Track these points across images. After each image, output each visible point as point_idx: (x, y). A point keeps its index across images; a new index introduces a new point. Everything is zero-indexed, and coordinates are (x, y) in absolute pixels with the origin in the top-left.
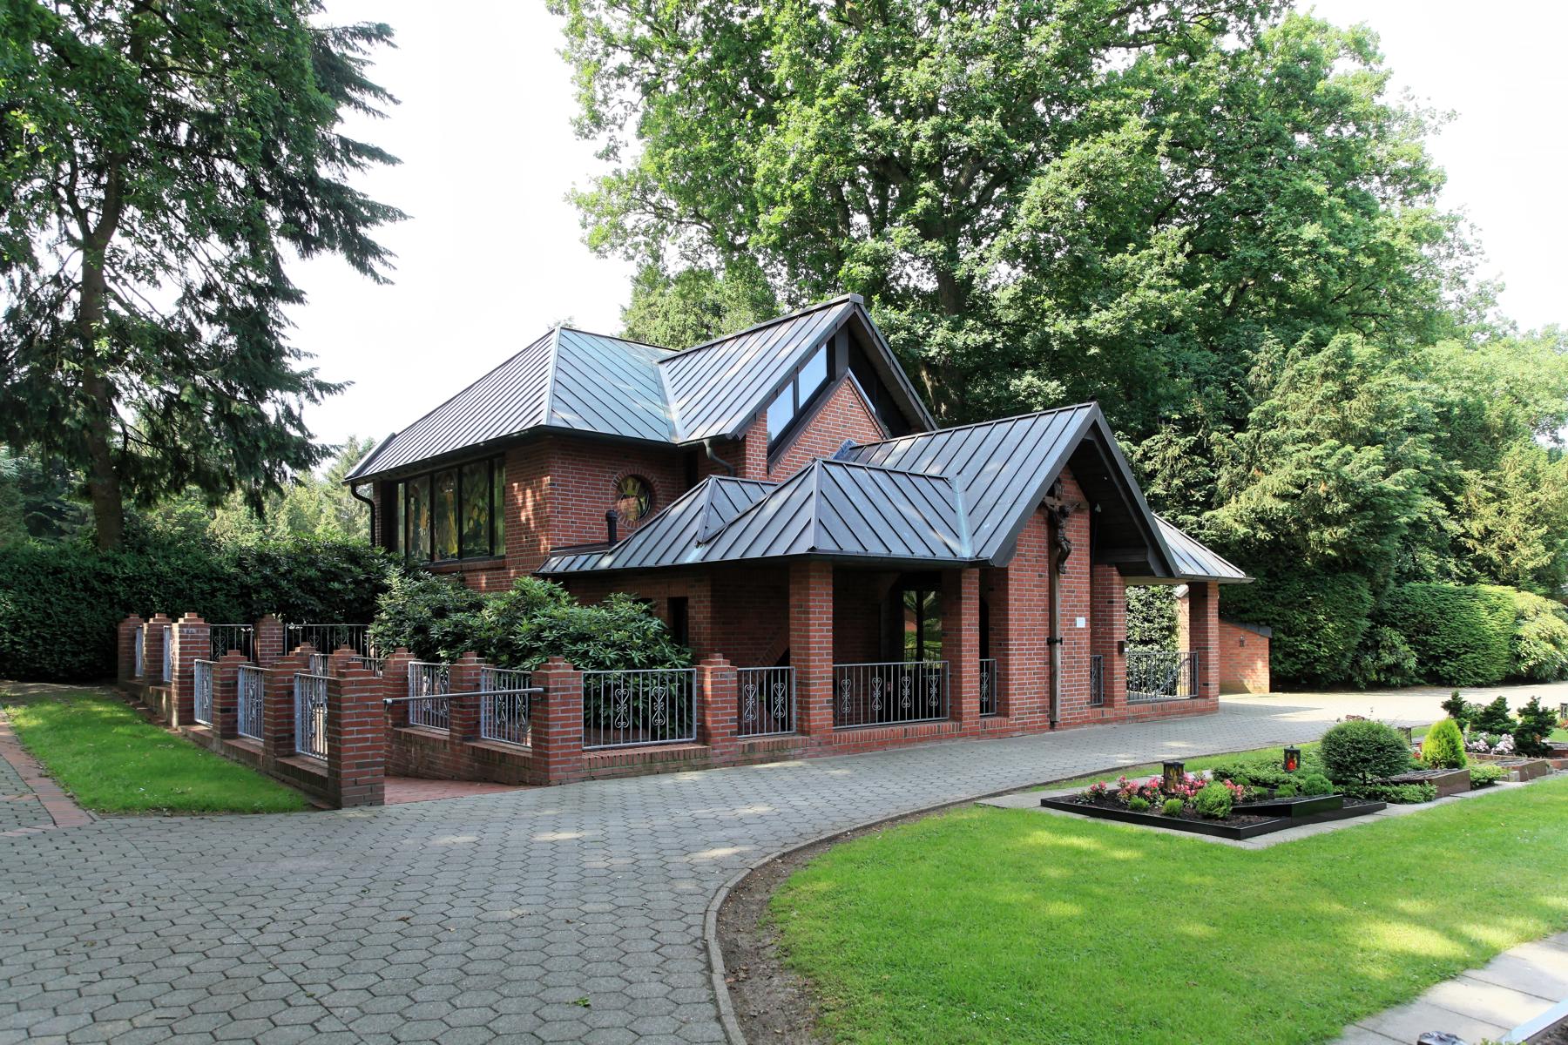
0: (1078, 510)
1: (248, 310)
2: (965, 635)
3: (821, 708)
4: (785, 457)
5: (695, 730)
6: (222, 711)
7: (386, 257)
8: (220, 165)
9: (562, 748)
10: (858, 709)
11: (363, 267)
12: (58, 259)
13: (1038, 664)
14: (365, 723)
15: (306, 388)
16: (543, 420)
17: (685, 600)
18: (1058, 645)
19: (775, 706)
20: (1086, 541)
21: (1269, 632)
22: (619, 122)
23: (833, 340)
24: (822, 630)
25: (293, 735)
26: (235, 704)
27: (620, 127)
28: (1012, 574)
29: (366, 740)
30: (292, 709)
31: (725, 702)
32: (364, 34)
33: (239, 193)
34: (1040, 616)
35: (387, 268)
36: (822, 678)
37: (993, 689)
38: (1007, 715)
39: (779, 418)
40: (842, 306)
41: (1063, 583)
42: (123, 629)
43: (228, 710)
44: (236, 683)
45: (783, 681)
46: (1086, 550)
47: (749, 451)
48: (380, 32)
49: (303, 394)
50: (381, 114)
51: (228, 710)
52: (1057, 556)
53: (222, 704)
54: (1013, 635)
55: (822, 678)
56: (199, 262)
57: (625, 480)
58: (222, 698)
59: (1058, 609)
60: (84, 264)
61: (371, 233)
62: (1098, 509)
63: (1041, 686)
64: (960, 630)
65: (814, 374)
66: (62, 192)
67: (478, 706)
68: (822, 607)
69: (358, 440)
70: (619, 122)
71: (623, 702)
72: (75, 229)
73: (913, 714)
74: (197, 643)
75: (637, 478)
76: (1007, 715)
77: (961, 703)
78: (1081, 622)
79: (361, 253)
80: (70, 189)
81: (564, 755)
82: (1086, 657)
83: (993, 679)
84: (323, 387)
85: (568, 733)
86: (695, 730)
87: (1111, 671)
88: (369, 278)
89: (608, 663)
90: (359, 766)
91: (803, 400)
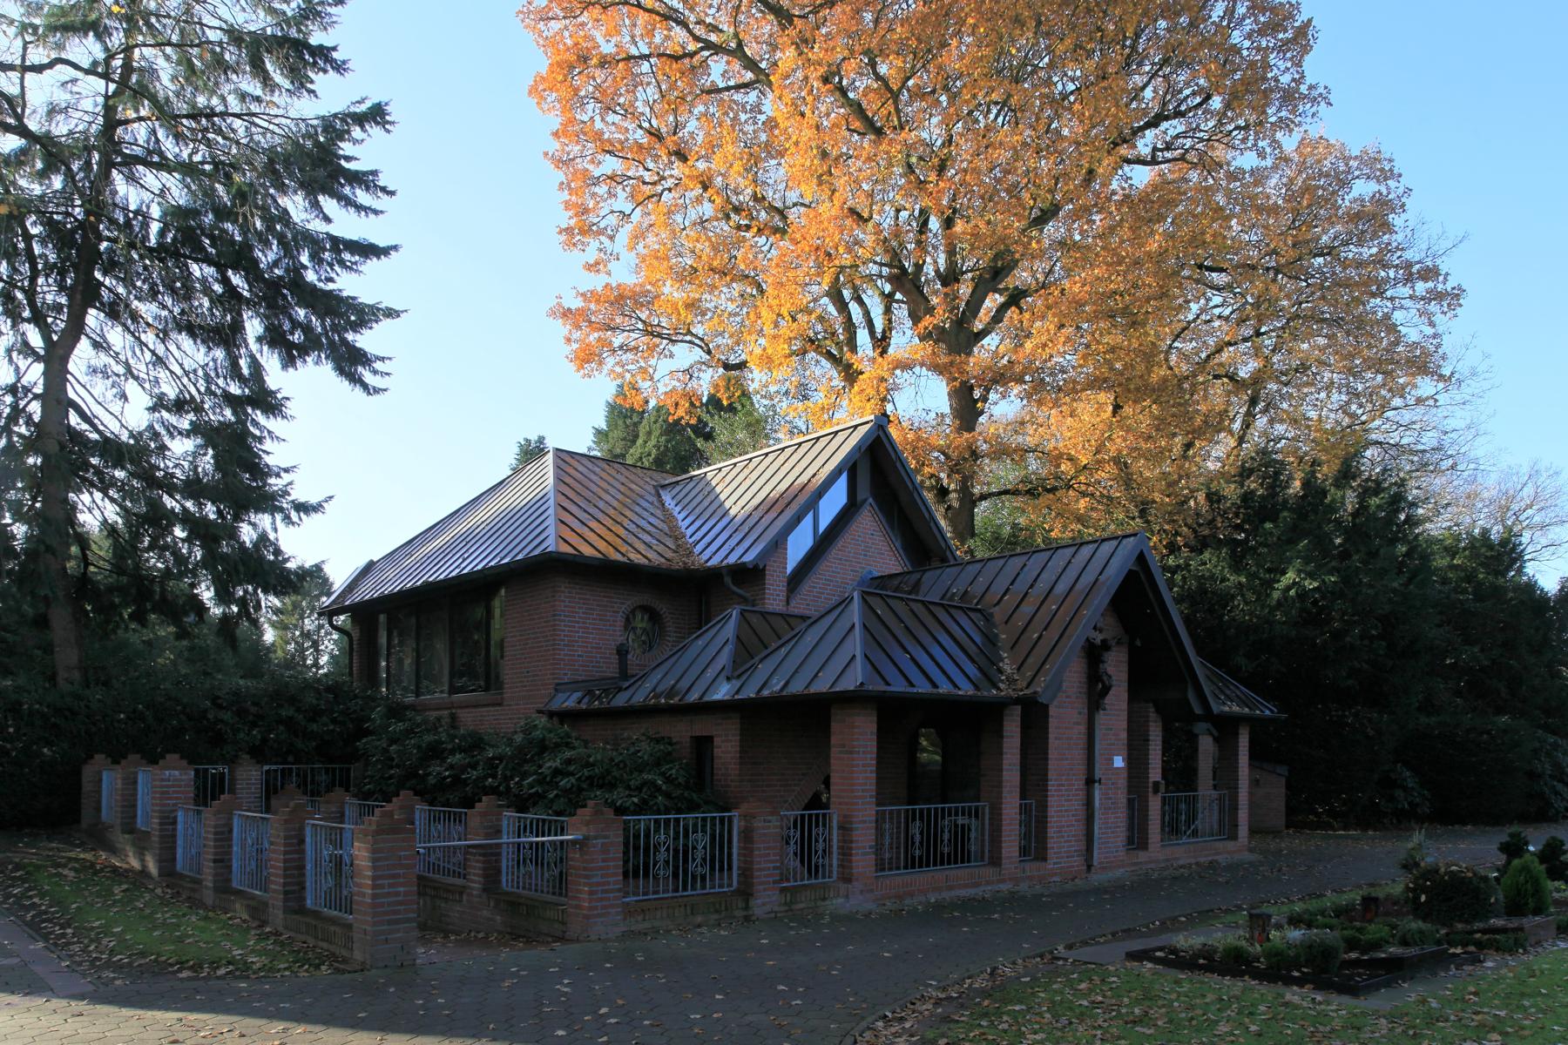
0: (1119, 643)
1: (224, 425)
2: (1006, 775)
3: (863, 854)
4: (805, 587)
5: (835, 873)
6: (215, 861)
7: (378, 365)
8: (195, 269)
9: (602, 899)
10: (898, 853)
11: (355, 380)
12: (12, 369)
13: (1077, 805)
14: (398, 876)
15: (281, 510)
16: (551, 545)
17: (710, 739)
18: (1097, 785)
19: (816, 852)
20: (1124, 676)
21: (1283, 770)
22: (609, 232)
23: (855, 464)
24: (866, 772)
25: (304, 888)
26: (230, 853)
27: (612, 238)
28: (1052, 711)
29: (398, 894)
30: (303, 859)
31: (768, 848)
32: (361, 119)
33: (216, 300)
34: (1079, 755)
35: (378, 377)
36: (865, 822)
37: (1030, 832)
38: (1045, 859)
39: (799, 544)
40: (868, 426)
41: (1101, 718)
42: (88, 772)
43: (221, 861)
44: (231, 831)
45: (824, 825)
46: (1125, 685)
47: (769, 580)
48: (376, 115)
49: (279, 517)
50: (376, 212)
51: (221, 861)
52: (1096, 690)
53: (216, 854)
54: (1052, 775)
55: (865, 822)
56: (171, 372)
57: (633, 612)
58: (215, 847)
59: (1097, 747)
60: (45, 373)
61: (364, 340)
62: (1138, 643)
63: (1078, 828)
64: (1001, 770)
65: (836, 500)
66: (19, 295)
67: (499, 854)
68: (866, 746)
70: (609, 232)
71: (663, 849)
72: (35, 339)
73: (942, 861)
74: (180, 786)
75: (645, 609)
77: (1001, 847)
78: (1119, 762)
79: (350, 362)
80: (31, 293)
81: (604, 907)
82: (1122, 798)
83: (1030, 821)
84: (303, 508)
85: (609, 884)
86: (835, 873)
88: (358, 390)
89: (632, 808)
90: (390, 922)
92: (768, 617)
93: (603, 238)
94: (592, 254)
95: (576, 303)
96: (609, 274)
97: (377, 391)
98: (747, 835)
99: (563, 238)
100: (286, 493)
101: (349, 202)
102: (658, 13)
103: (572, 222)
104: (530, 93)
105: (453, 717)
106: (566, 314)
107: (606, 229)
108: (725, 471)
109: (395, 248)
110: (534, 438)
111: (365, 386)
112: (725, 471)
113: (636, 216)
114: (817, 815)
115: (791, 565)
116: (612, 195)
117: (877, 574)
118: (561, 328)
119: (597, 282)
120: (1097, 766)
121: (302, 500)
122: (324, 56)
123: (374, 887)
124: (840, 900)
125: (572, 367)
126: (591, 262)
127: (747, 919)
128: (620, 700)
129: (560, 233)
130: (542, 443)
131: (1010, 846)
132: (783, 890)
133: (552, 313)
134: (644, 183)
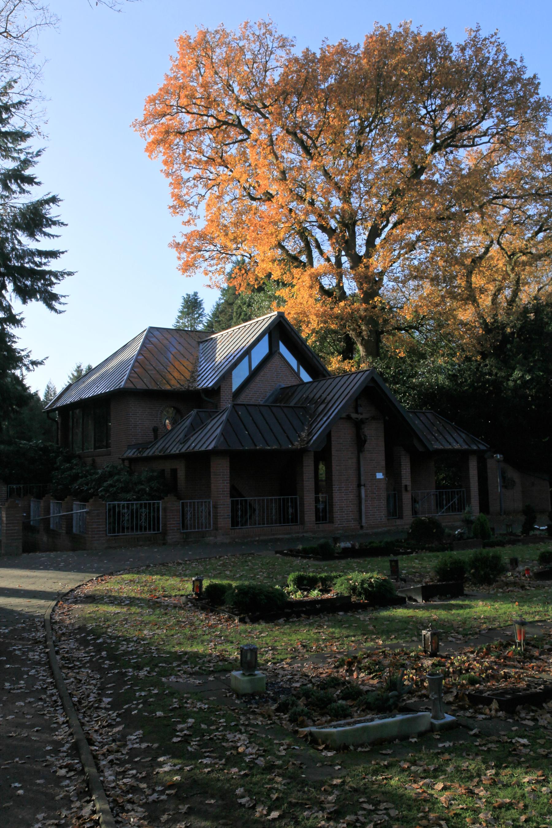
18: (362, 487)
22: (195, 204)
27: (196, 207)
32: (47, 202)
38: (333, 522)
48: (54, 200)
49: (24, 368)
59: (362, 469)
61: (55, 290)
62: (387, 418)
65: (262, 350)
69: (82, 367)
70: (195, 204)
76: (333, 522)
84: (34, 363)
87: (401, 500)
91: (254, 366)
92: (249, 408)
93: (192, 208)
94: (186, 217)
95: (181, 240)
96: (196, 225)
97: (60, 312)
98: (165, 510)
99: (171, 210)
100: (28, 356)
101: (46, 234)
102: (198, 114)
103: (175, 203)
104: (146, 151)
105: (94, 461)
106: (177, 245)
107: (193, 203)
108: (260, 322)
109: (66, 251)
110: (191, 293)
111: (56, 311)
112: (260, 322)
113: (208, 196)
114: (194, 503)
115: (235, 386)
116: (195, 186)
117: (284, 386)
118: (174, 253)
119: (188, 229)
120: (362, 478)
121: (34, 360)
122: (30, 180)
123: (6, 527)
124: (211, 538)
125: (180, 272)
126: (186, 220)
127: (164, 544)
128: (148, 453)
129: (170, 208)
130: (196, 296)
131: (310, 516)
132: (181, 533)
133: (170, 245)
134: (210, 180)
